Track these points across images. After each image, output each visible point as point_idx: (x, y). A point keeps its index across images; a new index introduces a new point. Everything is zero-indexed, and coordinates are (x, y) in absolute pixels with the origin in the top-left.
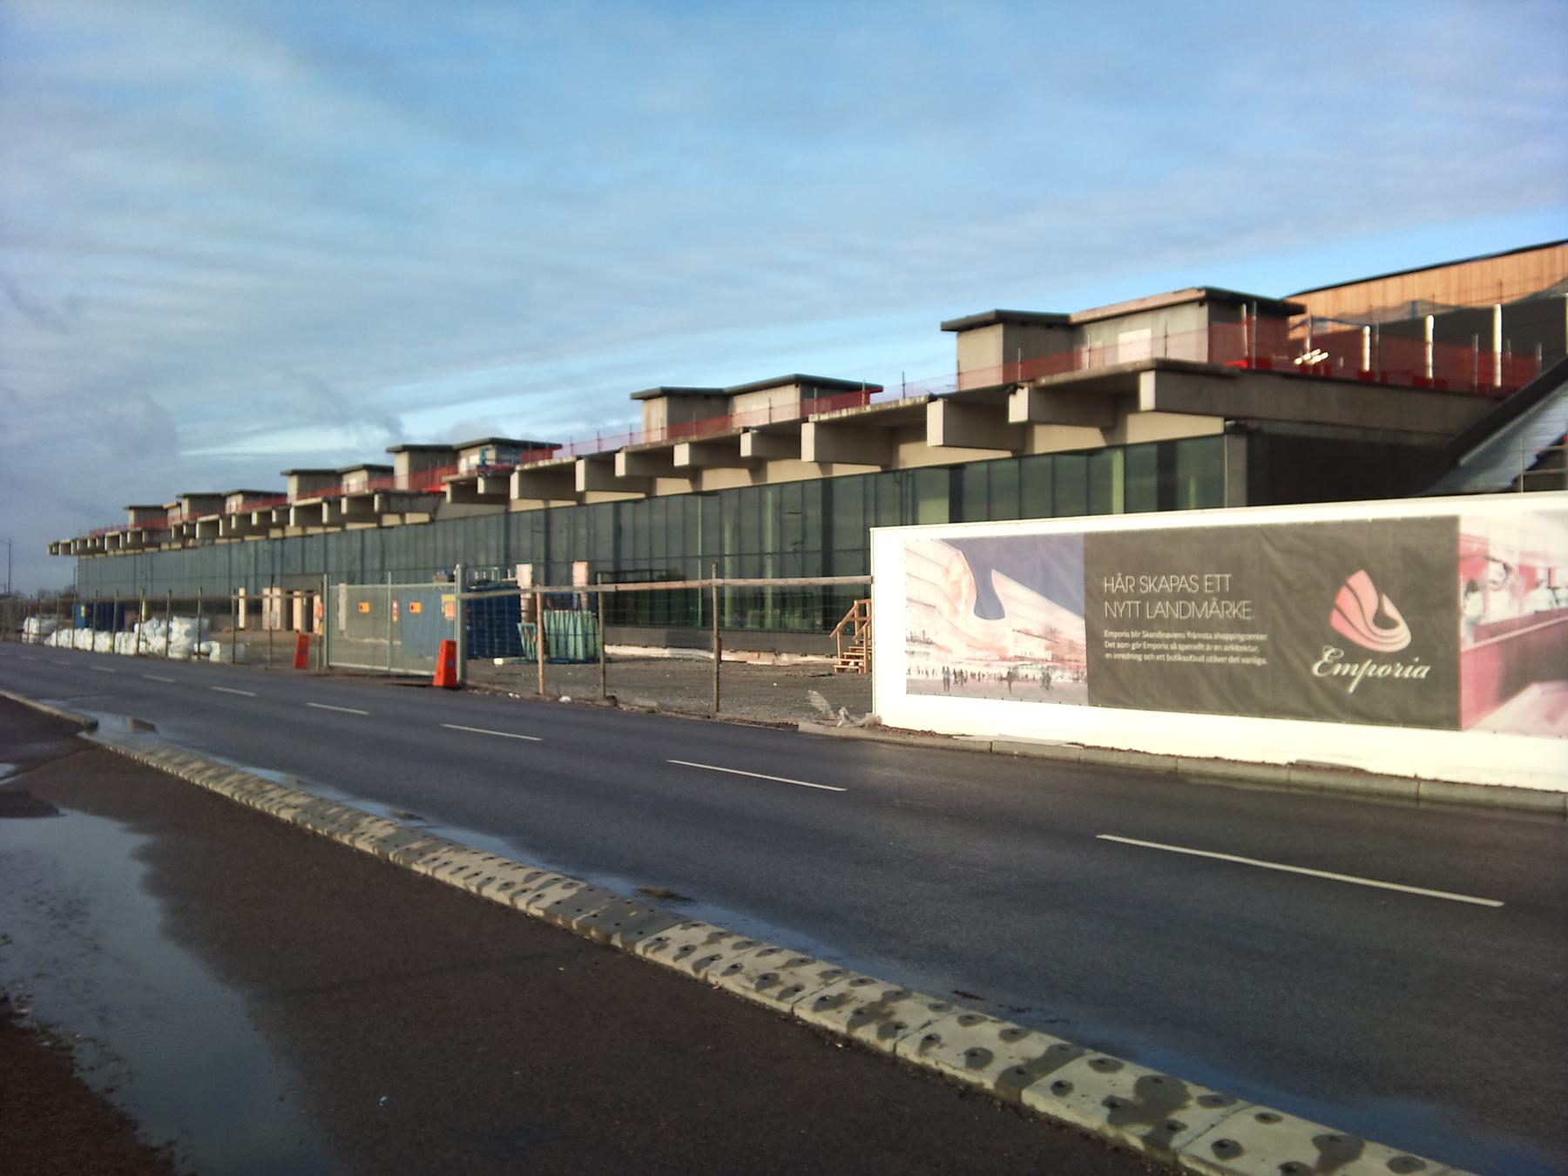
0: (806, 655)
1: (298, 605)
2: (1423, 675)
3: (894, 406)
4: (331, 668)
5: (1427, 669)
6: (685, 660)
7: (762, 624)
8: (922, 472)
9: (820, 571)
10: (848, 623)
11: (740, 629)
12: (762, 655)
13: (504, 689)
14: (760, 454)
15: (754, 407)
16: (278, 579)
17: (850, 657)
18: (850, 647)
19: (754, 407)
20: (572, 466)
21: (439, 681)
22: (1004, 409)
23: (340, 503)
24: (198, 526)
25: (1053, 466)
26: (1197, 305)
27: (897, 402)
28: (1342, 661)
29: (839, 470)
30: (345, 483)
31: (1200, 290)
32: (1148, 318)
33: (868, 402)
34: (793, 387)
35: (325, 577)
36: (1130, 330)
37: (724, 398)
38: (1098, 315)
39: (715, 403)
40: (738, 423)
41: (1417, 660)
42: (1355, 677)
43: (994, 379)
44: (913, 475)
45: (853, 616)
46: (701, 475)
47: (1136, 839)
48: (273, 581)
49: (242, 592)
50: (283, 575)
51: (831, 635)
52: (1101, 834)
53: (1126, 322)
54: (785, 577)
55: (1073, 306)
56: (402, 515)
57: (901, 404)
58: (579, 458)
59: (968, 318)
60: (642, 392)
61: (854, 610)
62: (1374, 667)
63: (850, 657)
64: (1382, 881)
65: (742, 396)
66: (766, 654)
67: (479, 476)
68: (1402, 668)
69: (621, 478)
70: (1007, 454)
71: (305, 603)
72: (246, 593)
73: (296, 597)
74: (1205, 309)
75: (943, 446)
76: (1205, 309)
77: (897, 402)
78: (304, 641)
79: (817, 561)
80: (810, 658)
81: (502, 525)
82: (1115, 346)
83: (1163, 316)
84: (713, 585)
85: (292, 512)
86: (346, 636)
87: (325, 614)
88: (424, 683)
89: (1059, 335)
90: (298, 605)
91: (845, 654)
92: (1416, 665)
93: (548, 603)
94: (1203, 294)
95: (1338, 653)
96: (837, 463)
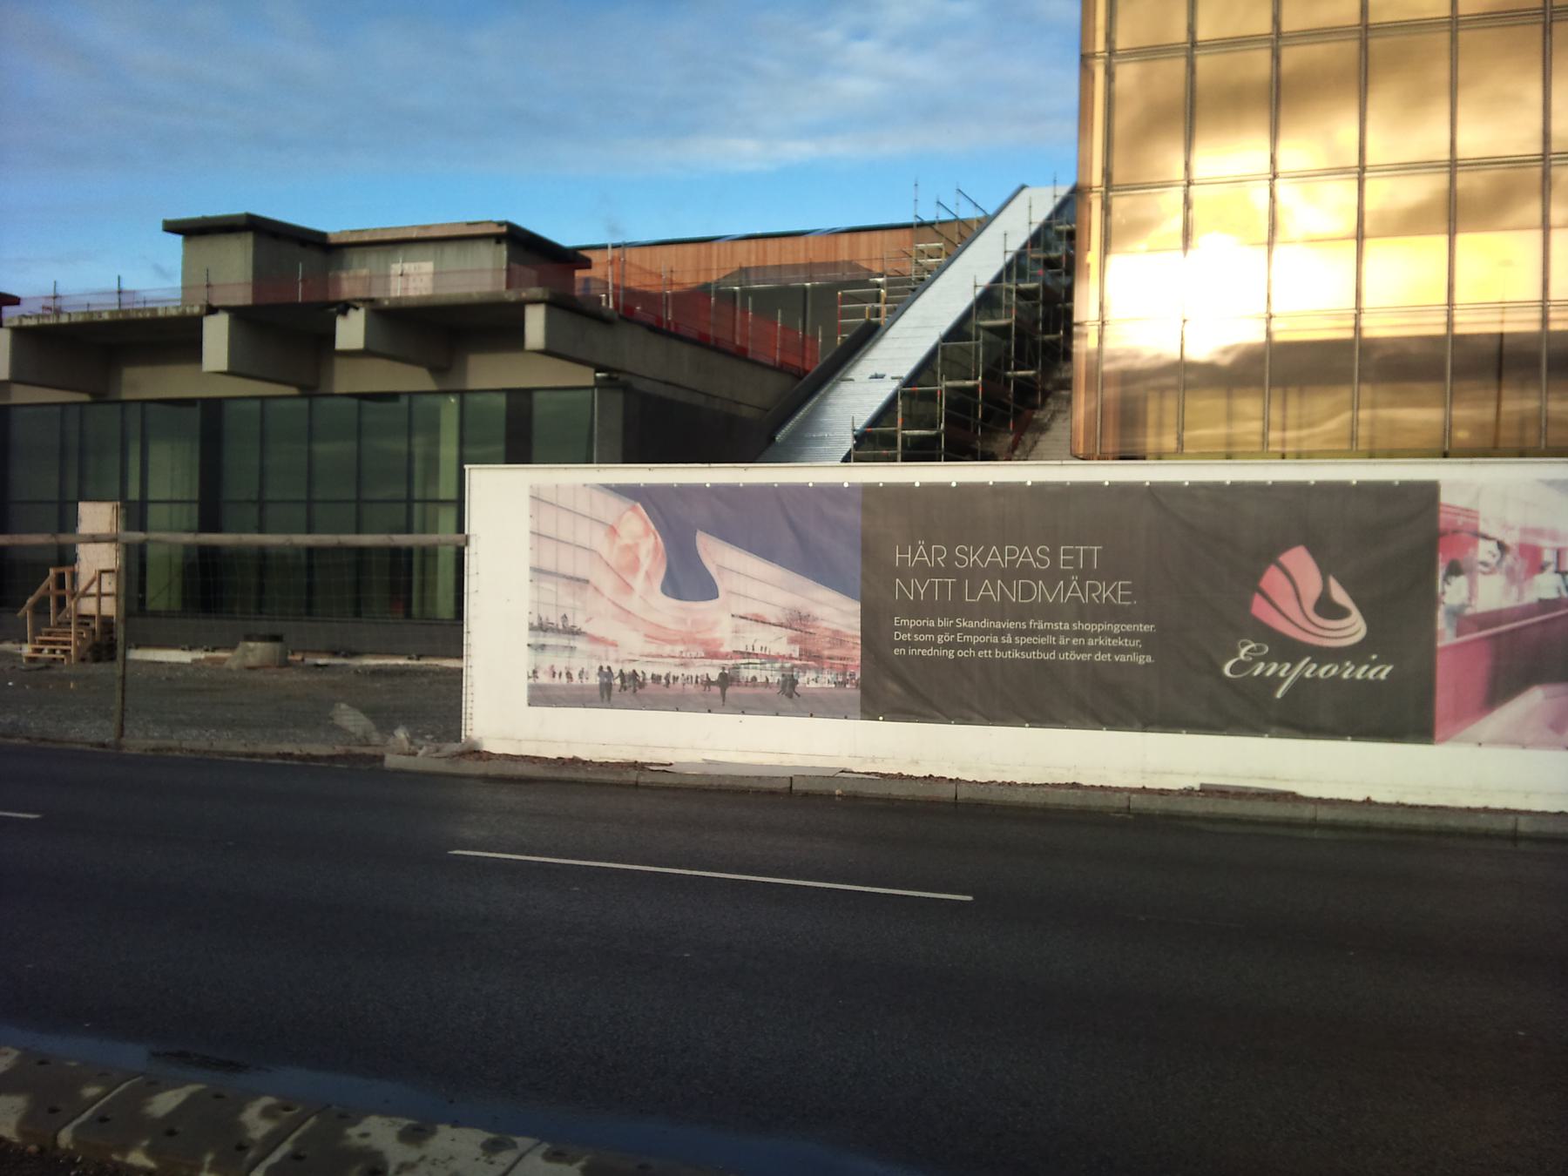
2: (1383, 676)
5: (1389, 669)
26: (493, 242)
28: (1267, 660)
31: (500, 224)
32: (431, 249)
41: (1374, 657)
42: (1284, 679)
45: (49, 588)
53: (400, 252)
58: (212, 310)
62: (1314, 666)
68: (1352, 668)
82: (387, 276)
83: (450, 251)
92: (1373, 664)
94: (504, 229)
95: (1260, 649)
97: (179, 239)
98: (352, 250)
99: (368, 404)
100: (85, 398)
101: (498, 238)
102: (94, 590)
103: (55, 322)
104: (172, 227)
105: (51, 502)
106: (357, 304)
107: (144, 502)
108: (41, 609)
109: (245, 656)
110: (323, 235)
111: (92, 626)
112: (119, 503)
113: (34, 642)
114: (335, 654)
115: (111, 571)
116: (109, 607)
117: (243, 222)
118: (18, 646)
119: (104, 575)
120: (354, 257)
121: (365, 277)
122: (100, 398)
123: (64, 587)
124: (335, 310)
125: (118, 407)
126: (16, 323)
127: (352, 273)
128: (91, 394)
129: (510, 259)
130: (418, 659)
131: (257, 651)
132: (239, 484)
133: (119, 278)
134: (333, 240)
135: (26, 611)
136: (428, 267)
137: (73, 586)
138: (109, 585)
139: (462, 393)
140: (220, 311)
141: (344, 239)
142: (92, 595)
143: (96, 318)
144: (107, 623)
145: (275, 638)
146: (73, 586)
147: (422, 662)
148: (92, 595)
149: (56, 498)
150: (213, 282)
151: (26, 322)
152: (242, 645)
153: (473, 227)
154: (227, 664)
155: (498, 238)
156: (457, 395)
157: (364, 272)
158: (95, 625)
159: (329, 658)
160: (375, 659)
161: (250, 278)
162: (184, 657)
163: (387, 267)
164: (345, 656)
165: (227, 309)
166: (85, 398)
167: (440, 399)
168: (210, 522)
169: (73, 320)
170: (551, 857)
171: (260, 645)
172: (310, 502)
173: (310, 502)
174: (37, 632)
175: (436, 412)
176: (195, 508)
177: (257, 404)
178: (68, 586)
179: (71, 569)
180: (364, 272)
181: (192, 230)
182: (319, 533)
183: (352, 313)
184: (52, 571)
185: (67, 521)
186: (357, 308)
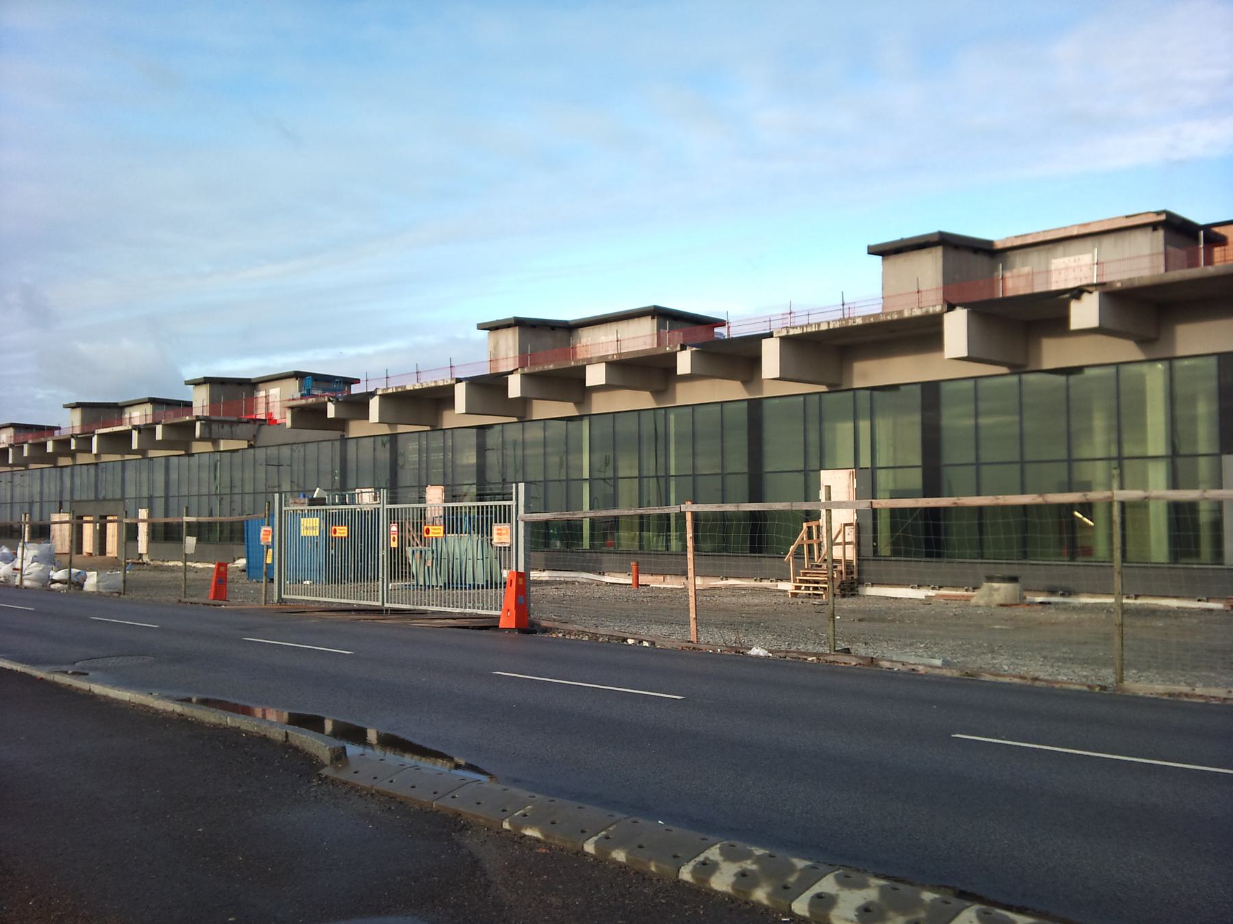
0: (727, 578)
1: (88, 530)
3: (895, 317)
4: (281, 600)
6: (566, 583)
7: (668, 548)
8: (701, 409)
9: (747, 498)
10: (799, 545)
11: (639, 552)
12: (668, 577)
13: (805, 657)
14: (342, 416)
15: (603, 339)
16: (66, 505)
17: (801, 581)
18: (801, 571)
19: (603, 339)
20: (451, 388)
21: (508, 621)
22: (505, 388)
23: (155, 429)
24: (95, 439)
25: (976, 388)
26: (1150, 230)
27: (901, 312)
29: (402, 429)
30: (127, 416)
31: (1158, 213)
32: (1089, 242)
33: (1209, 261)
34: (149, 404)
35: (277, 496)
36: (1064, 256)
37: (569, 329)
38: (1030, 240)
39: (560, 334)
40: (582, 354)
43: (150, 421)
44: (396, 437)
45: (803, 539)
46: (590, 399)
47: (1109, 754)
48: (60, 508)
49: (143, 514)
50: (72, 501)
51: (786, 560)
52: (955, 734)
53: (1060, 248)
54: (697, 503)
55: (997, 232)
56: (215, 442)
57: (906, 314)
58: (459, 380)
59: (902, 240)
60: (192, 380)
61: (803, 534)
63: (801, 581)
64: (1103, 753)
65: (5, 429)
66: (673, 577)
67: (330, 400)
69: (159, 441)
70: (515, 420)
71: (98, 528)
72: (150, 515)
73: (111, 521)
74: (1160, 233)
75: (379, 423)
76: (1160, 233)
77: (901, 312)
78: (222, 569)
79: (741, 484)
80: (732, 582)
81: (58, 478)
82: (1048, 272)
83: (1108, 242)
84: (1115, 498)
85: (95, 439)
86: (146, 559)
87: (277, 538)
88: (490, 625)
89: (981, 261)
90: (88, 530)
91: (798, 578)
93: (579, 528)
94: (1163, 217)
96: (104, 454)
97: (880, 258)
98: (1015, 252)
99: (876, 393)
100: (823, 388)
101: (1154, 226)
102: (840, 540)
103: (801, 332)
104: (874, 251)
105: (162, 497)
106: (1090, 289)
107: (874, 469)
108: (798, 554)
109: (991, 595)
110: (990, 243)
111: (839, 568)
112: (854, 470)
113: (795, 581)
114: (1052, 592)
115: (850, 524)
116: (851, 554)
117: (936, 239)
118: (774, 583)
119: (846, 527)
120: (1017, 258)
121: (1028, 275)
122: (835, 388)
123: (813, 539)
124: (1067, 296)
125: (442, 432)
126: (784, 333)
127: (1015, 271)
128: (431, 426)
129: (1166, 243)
130: (1136, 599)
131: (1002, 591)
132: (955, 453)
133: (843, 293)
134: (999, 246)
135: (789, 557)
136: (278, 389)
137: (818, 538)
138: (850, 536)
139: (1171, 359)
140: (958, 308)
141: (1009, 244)
142: (839, 544)
143: (850, 323)
144: (848, 564)
145: (1013, 579)
146: (818, 538)
147: (1140, 601)
148: (839, 544)
149: (869, 466)
150: (921, 289)
151: (792, 332)
152: (986, 586)
153: (1131, 219)
154: (973, 601)
155: (1154, 226)
156: (1166, 363)
157: (1026, 270)
158: (842, 567)
159: (1047, 596)
160: (1093, 597)
161: (942, 285)
162: (920, 594)
163: (1048, 263)
164: (1062, 595)
165: (466, 379)
166: (823, 388)
167: (1145, 368)
168: (932, 487)
169: (831, 327)
170: (1098, 757)
171: (1003, 585)
172: (978, 464)
173: (1022, 463)
174: (797, 574)
175: (1141, 378)
176: (746, 477)
177: (971, 384)
178: (815, 538)
179: (816, 523)
180: (1026, 270)
181: (886, 251)
182: (1184, 488)
183: (1085, 296)
184: (805, 525)
185: (810, 489)
186: (1091, 292)
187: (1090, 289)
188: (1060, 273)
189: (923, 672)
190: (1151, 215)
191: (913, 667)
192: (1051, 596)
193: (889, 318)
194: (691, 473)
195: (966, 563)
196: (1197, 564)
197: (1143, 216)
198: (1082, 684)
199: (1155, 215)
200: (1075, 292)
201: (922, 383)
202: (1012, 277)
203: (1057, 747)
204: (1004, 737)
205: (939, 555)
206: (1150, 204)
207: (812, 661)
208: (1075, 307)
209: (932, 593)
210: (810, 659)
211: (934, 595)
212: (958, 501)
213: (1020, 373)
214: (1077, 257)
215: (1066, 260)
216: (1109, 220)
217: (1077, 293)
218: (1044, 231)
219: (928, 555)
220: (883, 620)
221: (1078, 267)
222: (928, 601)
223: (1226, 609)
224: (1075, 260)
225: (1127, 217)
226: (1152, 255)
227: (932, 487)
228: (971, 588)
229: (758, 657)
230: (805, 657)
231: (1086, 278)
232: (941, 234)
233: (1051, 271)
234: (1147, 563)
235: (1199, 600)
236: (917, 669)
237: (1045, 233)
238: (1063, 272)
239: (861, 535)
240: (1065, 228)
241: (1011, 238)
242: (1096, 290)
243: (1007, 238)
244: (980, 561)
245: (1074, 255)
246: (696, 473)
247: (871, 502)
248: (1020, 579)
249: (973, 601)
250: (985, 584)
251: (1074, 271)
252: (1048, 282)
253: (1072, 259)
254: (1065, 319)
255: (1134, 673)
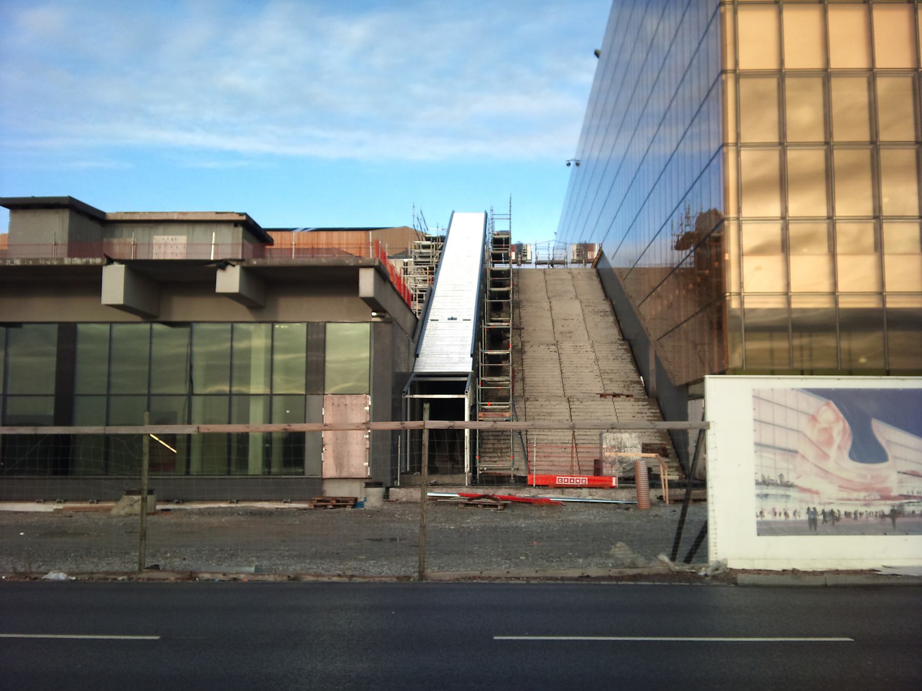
3: (55, 263)
13: (114, 577)
26: (232, 226)
31: (241, 214)
32: (185, 228)
38: (137, 217)
53: (161, 228)
55: (110, 206)
74: (240, 230)
89: (95, 227)
94: (244, 218)
97: (7, 211)
101: (236, 223)
110: (104, 214)
117: (66, 202)
120: (125, 230)
127: (122, 240)
141: (119, 218)
147: (239, 505)
154: (114, 512)
163: (150, 238)
164: (178, 503)
186: (234, 266)
187: (233, 263)
188: (160, 247)
189: (246, 580)
190: (235, 215)
191: (234, 576)
192: (167, 504)
193: (49, 263)
194: (105, 393)
195: (159, 479)
196: (174, 475)
197: (229, 215)
198: (394, 576)
199: (238, 215)
200: (221, 264)
201: (59, 323)
202: (119, 244)
203: (665, 641)
204: (527, 634)
205: (66, 473)
206: (234, 206)
207: (123, 580)
208: (221, 276)
209: (60, 506)
210: (120, 578)
211: (51, 510)
212: (288, 427)
213: (152, 322)
214: (174, 237)
215: (166, 237)
216: (202, 213)
217: (223, 264)
218: (149, 213)
219: (55, 473)
220: (64, 533)
221: (175, 244)
222: (58, 511)
223: (310, 508)
224: (172, 239)
225: (217, 213)
226: (232, 244)
227: (64, 415)
228: (95, 501)
229: (59, 583)
230: (114, 577)
231: (181, 254)
232: (71, 199)
233: (153, 244)
234: (247, 475)
235: (285, 502)
236: (238, 578)
237: (150, 214)
238: (162, 246)
239: (226, 456)
240: (167, 213)
241: (121, 213)
242: (237, 264)
243: (117, 213)
244: (227, 477)
245: (172, 235)
246: (228, 392)
247: (198, 428)
248: (154, 492)
249: (114, 512)
250: (126, 497)
251: (171, 247)
252: (150, 252)
253: (170, 237)
254: (212, 283)
255: (374, 563)
